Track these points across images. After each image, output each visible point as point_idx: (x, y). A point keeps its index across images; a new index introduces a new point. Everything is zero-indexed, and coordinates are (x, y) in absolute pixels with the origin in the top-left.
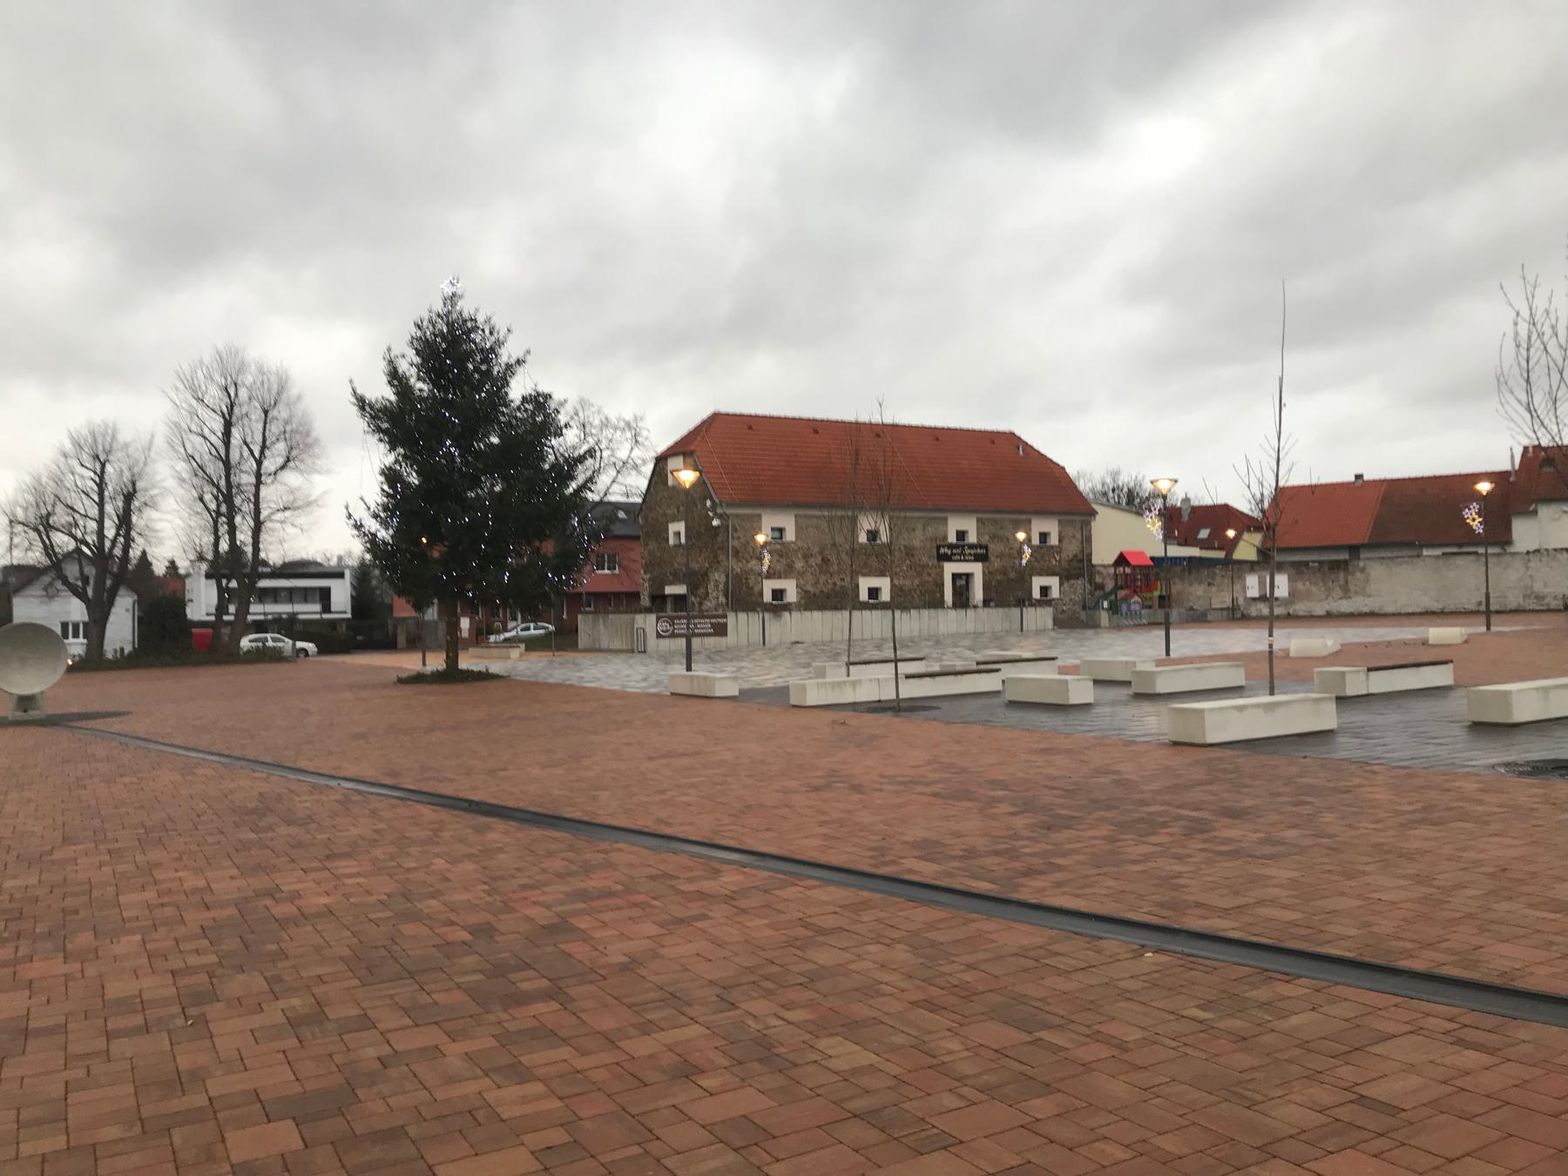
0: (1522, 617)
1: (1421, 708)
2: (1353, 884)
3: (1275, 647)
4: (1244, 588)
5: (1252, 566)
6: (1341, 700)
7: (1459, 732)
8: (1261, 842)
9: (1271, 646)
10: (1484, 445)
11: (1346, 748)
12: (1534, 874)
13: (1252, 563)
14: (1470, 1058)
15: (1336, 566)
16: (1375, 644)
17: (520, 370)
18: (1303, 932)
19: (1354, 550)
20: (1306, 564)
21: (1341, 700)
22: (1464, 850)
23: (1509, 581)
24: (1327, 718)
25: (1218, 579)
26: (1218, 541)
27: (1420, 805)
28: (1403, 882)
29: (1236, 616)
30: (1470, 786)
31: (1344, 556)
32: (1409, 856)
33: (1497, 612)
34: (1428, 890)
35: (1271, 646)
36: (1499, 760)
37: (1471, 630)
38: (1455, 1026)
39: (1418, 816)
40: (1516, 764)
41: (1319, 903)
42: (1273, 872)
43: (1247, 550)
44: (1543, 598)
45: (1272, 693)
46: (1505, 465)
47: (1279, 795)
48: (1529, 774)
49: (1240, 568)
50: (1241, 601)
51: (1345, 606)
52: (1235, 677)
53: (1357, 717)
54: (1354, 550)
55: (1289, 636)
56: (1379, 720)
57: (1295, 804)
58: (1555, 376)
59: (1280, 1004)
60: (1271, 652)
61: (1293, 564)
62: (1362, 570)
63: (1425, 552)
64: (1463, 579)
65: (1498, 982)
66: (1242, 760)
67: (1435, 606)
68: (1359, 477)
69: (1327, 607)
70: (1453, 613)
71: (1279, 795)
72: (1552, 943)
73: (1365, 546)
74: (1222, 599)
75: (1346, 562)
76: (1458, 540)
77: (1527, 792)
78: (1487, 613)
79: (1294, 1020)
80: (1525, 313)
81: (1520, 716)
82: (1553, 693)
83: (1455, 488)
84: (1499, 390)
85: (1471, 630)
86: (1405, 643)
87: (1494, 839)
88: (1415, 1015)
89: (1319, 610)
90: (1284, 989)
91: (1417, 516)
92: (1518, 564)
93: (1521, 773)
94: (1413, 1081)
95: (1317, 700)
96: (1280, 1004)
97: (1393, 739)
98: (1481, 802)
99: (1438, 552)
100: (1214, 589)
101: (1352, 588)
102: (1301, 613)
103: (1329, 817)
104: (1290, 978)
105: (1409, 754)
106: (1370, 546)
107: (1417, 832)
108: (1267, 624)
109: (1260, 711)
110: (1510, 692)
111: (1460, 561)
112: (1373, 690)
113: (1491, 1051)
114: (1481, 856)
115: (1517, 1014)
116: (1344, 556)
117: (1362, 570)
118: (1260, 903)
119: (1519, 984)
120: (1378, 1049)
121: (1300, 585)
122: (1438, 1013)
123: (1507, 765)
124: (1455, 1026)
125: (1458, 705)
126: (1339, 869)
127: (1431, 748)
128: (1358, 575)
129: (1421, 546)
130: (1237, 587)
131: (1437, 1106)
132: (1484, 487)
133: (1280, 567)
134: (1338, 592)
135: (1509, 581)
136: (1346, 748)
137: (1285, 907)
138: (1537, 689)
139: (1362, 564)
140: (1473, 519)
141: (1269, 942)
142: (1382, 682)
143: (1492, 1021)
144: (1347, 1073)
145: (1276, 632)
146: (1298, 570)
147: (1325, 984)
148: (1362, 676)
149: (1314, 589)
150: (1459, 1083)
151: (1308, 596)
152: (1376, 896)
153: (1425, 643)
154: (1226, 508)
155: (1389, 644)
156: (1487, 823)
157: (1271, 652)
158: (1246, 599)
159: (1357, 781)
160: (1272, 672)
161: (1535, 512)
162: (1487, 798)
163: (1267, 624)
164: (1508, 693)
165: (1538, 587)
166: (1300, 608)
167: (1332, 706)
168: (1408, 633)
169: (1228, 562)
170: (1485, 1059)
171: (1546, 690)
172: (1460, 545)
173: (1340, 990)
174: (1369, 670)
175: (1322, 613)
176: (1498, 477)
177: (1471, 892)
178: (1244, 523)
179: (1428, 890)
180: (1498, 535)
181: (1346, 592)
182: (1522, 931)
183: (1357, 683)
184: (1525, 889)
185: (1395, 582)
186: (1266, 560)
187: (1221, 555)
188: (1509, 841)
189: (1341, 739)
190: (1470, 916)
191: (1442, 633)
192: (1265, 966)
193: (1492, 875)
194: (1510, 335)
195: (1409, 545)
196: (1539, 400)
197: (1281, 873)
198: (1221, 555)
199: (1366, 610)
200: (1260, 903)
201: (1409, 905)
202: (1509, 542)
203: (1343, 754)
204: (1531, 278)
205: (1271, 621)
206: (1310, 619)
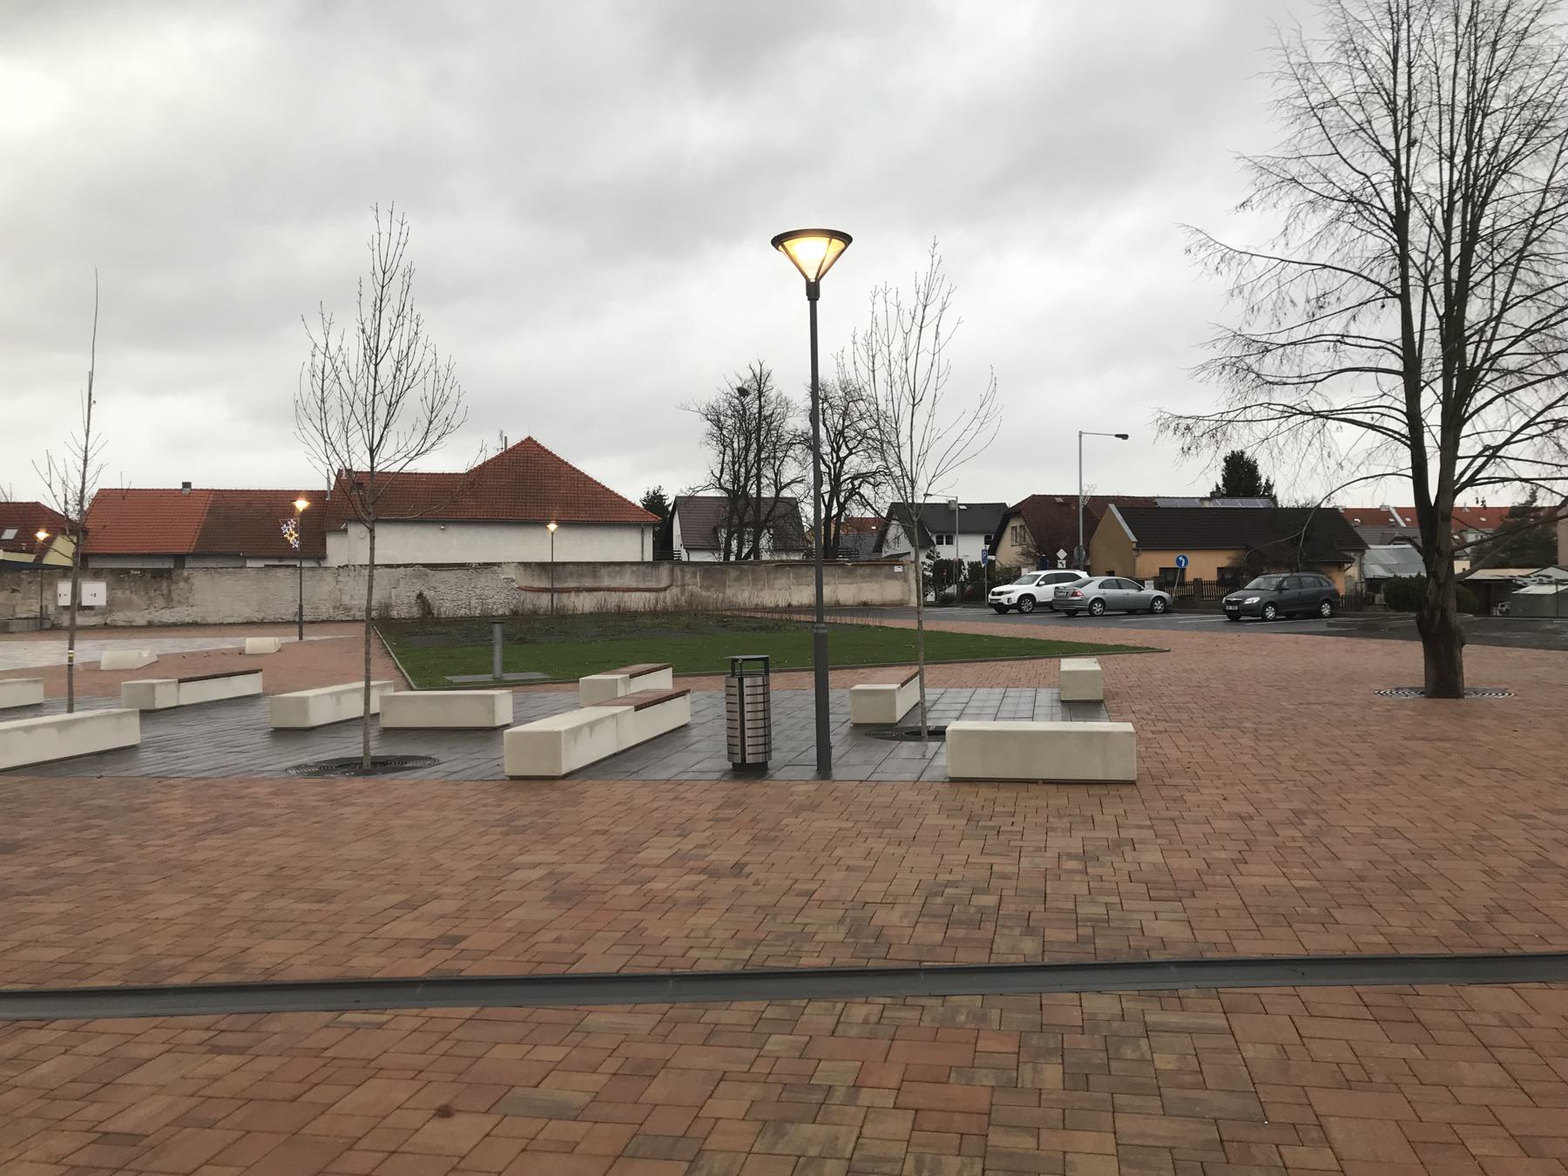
0: (333, 627)
1: (229, 718)
2: (128, 906)
3: (75, 661)
4: (55, 596)
5: (65, 572)
6: (147, 714)
7: (260, 739)
8: (39, 875)
9: (71, 659)
10: (296, 467)
11: (150, 762)
12: (307, 870)
13: (65, 568)
14: (224, 1062)
15: (159, 574)
16: (193, 654)
17: (822, 282)
18: (68, 968)
19: (180, 559)
20: (127, 571)
21: (147, 714)
22: (248, 854)
23: (321, 592)
24: (130, 733)
25: (25, 584)
26: (25, 542)
27: (213, 815)
28: (185, 896)
29: (43, 625)
30: (261, 791)
31: (169, 565)
32: (190, 868)
33: (311, 622)
34: (206, 901)
35: (71, 659)
36: (290, 764)
37: (285, 640)
38: (211, 1034)
39: (208, 827)
40: (306, 766)
41: (89, 934)
42: (37, 908)
43: (62, 552)
44: (350, 609)
45: (70, 710)
46: (323, 486)
47: (64, 821)
48: (316, 774)
49: (44, 573)
50: (51, 609)
51: (167, 616)
52: (32, 693)
53: (164, 730)
54: (180, 559)
55: (103, 647)
56: (186, 732)
57: (79, 830)
58: (348, 409)
59: (30, 1055)
60: (70, 666)
61: (113, 570)
62: (186, 580)
63: (249, 564)
64: (279, 590)
65: (259, 979)
66: (23, 787)
67: (257, 617)
68: (187, 485)
69: (149, 617)
70: (274, 623)
71: (64, 821)
72: (314, 932)
73: (189, 555)
74: (27, 606)
75: (169, 570)
76: (274, 552)
77: (312, 791)
78: (300, 623)
79: (44, 1069)
80: (322, 345)
81: (316, 719)
82: (343, 697)
83: (275, 503)
84: (297, 416)
85: (285, 640)
86: (224, 653)
87: (277, 840)
88: (171, 1033)
89: (140, 620)
90: (34, 1037)
91: (239, 528)
92: (329, 577)
93: (310, 774)
94: (163, 1100)
95: (119, 715)
96: (30, 1055)
97: (199, 752)
98: (270, 806)
99: (261, 564)
100: (19, 595)
101: (175, 597)
102: (120, 623)
103: (117, 839)
104: (44, 1023)
105: (211, 763)
106: (197, 556)
107: (207, 843)
108: (68, 635)
109: (53, 731)
110: (307, 698)
111: (280, 573)
112: (182, 703)
113: (241, 1051)
114: (262, 859)
115: (269, 1008)
116: (169, 565)
117: (186, 580)
118: (24, 944)
119: (277, 979)
120: (130, 1078)
121: (119, 594)
122: (195, 1025)
123: (298, 767)
124: (211, 1034)
125: (264, 715)
126: (119, 892)
127: (231, 757)
128: (182, 584)
129: (245, 558)
130: (48, 594)
131: (181, 1122)
132: (301, 505)
133: (97, 575)
134: (160, 602)
135: (321, 592)
136: (150, 762)
137: (52, 944)
138: (331, 694)
139: (185, 574)
140: (293, 538)
141: (27, 987)
142: (194, 693)
143: (247, 1020)
144: (93, 1112)
145: (77, 645)
146: (117, 577)
147: (82, 1021)
148: (173, 688)
149: (135, 598)
150: (207, 1092)
151: (128, 605)
152: (154, 915)
153: (241, 653)
154: (37, 506)
155: (208, 654)
156: (273, 825)
157: (70, 666)
158: (57, 607)
159: (152, 797)
160: (71, 687)
161: (345, 531)
162: (276, 801)
163: (812, 573)
164: (305, 699)
165: (346, 600)
166: (119, 617)
167: (136, 721)
168: (227, 643)
169: (37, 567)
170: (235, 1060)
171: (338, 695)
172: (281, 558)
173: (97, 1025)
174: (180, 681)
175: (143, 623)
176: (312, 495)
177: (246, 896)
178: (58, 524)
179: (206, 901)
180: (313, 549)
181: (169, 602)
182: (288, 926)
183: (168, 695)
184: (298, 884)
185: (217, 592)
186: (84, 565)
187: (29, 558)
188: (290, 840)
189: (143, 755)
190: (244, 919)
191: (257, 643)
192: (18, 1015)
193: (269, 875)
194: (308, 366)
195: (235, 556)
196: (334, 429)
197: (52, 907)
198: (29, 558)
199: (188, 620)
200: (24, 944)
201: (188, 919)
202: (324, 557)
203: (144, 770)
204: (327, 318)
205: (72, 633)
206: (130, 629)
